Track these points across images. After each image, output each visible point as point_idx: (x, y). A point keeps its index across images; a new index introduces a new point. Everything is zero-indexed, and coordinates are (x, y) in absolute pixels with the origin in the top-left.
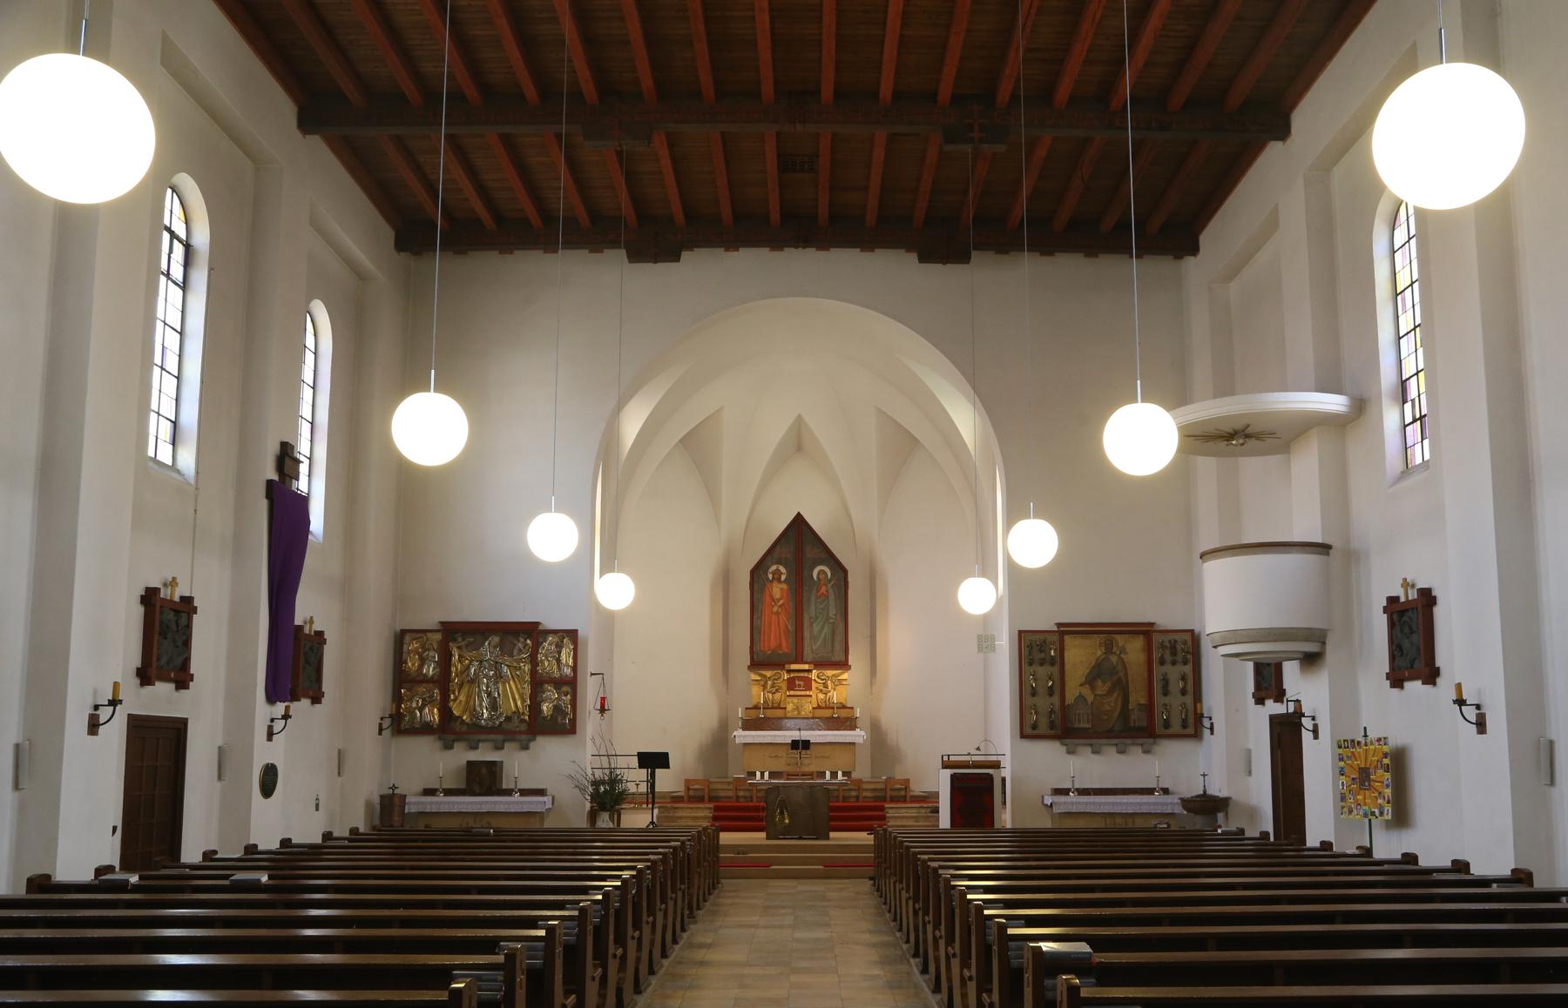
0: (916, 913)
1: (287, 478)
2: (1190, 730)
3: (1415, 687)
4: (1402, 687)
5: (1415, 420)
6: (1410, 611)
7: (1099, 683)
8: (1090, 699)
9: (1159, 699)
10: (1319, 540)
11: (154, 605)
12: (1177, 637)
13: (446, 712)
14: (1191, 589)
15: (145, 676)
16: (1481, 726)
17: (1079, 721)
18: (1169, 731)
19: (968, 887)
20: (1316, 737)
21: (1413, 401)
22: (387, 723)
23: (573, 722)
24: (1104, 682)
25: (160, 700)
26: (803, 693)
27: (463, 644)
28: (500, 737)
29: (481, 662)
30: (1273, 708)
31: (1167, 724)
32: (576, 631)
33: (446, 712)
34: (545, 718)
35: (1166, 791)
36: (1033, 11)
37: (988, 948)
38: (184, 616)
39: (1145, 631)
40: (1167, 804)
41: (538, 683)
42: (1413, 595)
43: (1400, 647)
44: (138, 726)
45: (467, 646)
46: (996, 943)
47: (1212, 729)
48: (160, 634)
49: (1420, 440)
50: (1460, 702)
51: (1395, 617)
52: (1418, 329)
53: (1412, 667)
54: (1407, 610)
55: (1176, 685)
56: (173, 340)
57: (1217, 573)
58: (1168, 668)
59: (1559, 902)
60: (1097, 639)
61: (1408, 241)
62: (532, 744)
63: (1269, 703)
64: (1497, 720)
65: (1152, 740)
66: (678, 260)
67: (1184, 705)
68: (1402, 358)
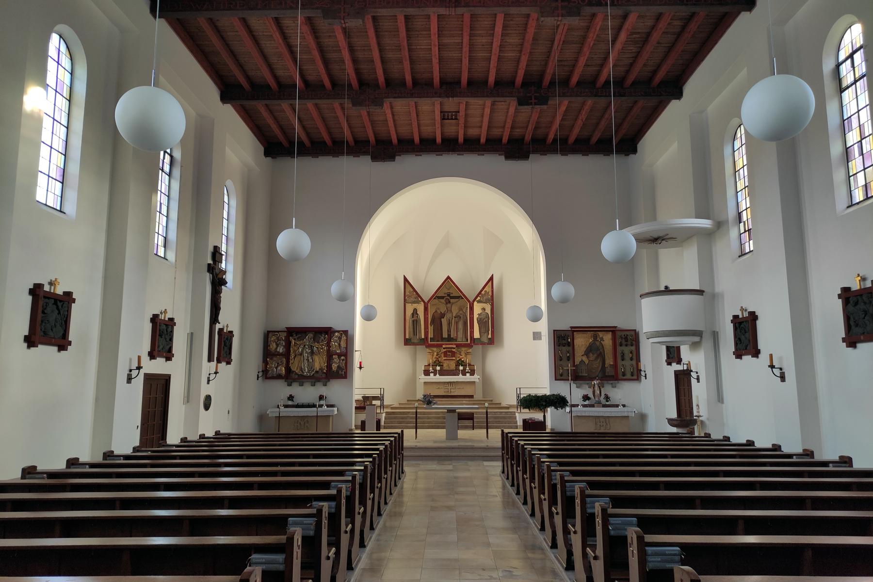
0: (512, 465)
1: (217, 262)
2: (635, 377)
3: (747, 358)
4: (741, 358)
5: (745, 231)
6: (745, 323)
7: (591, 355)
8: (587, 362)
9: (620, 363)
10: (698, 288)
11: (157, 323)
12: (628, 333)
13: (288, 370)
14: (636, 310)
15: (152, 355)
16: (783, 378)
17: (582, 372)
18: (625, 377)
19: (532, 448)
20: (698, 381)
21: (744, 222)
22: (260, 374)
23: (346, 373)
24: (593, 354)
25: (158, 366)
26: (451, 358)
27: (296, 337)
28: (313, 380)
29: (304, 346)
30: (676, 367)
31: (624, 374)
32: (347, 331)
33: (288, 370)
34: (334, 371)
35: (624, 406)
36: (561, 43)
37: (555, 485)
38: (170, 327)
39: (613, 330)
40: (624, 412)
41: (330, 356)
42: (746, 315)
43: (740, 339)
44: (149, 378)
45: (298, 338)
46: (559, 484)
47: (645, 376)
48: (159, 335)
49: (748, 241)
50: (772, 367)
51: (737, 325)
52: (746, 188)
53: (746, 349)
54: (743, 322)
55: (628, 356)
56: (164, 200)
57: (647, 304)
58: (624, 348)
59: (828, 466)
60: (589, 334)
61: (741, 146)
62: (328, 383)
63: (674, 364)
64: (790, 375)
65: (617, 382)
66: (394, 161)
67: (632, 365)
68: (739, 201)
